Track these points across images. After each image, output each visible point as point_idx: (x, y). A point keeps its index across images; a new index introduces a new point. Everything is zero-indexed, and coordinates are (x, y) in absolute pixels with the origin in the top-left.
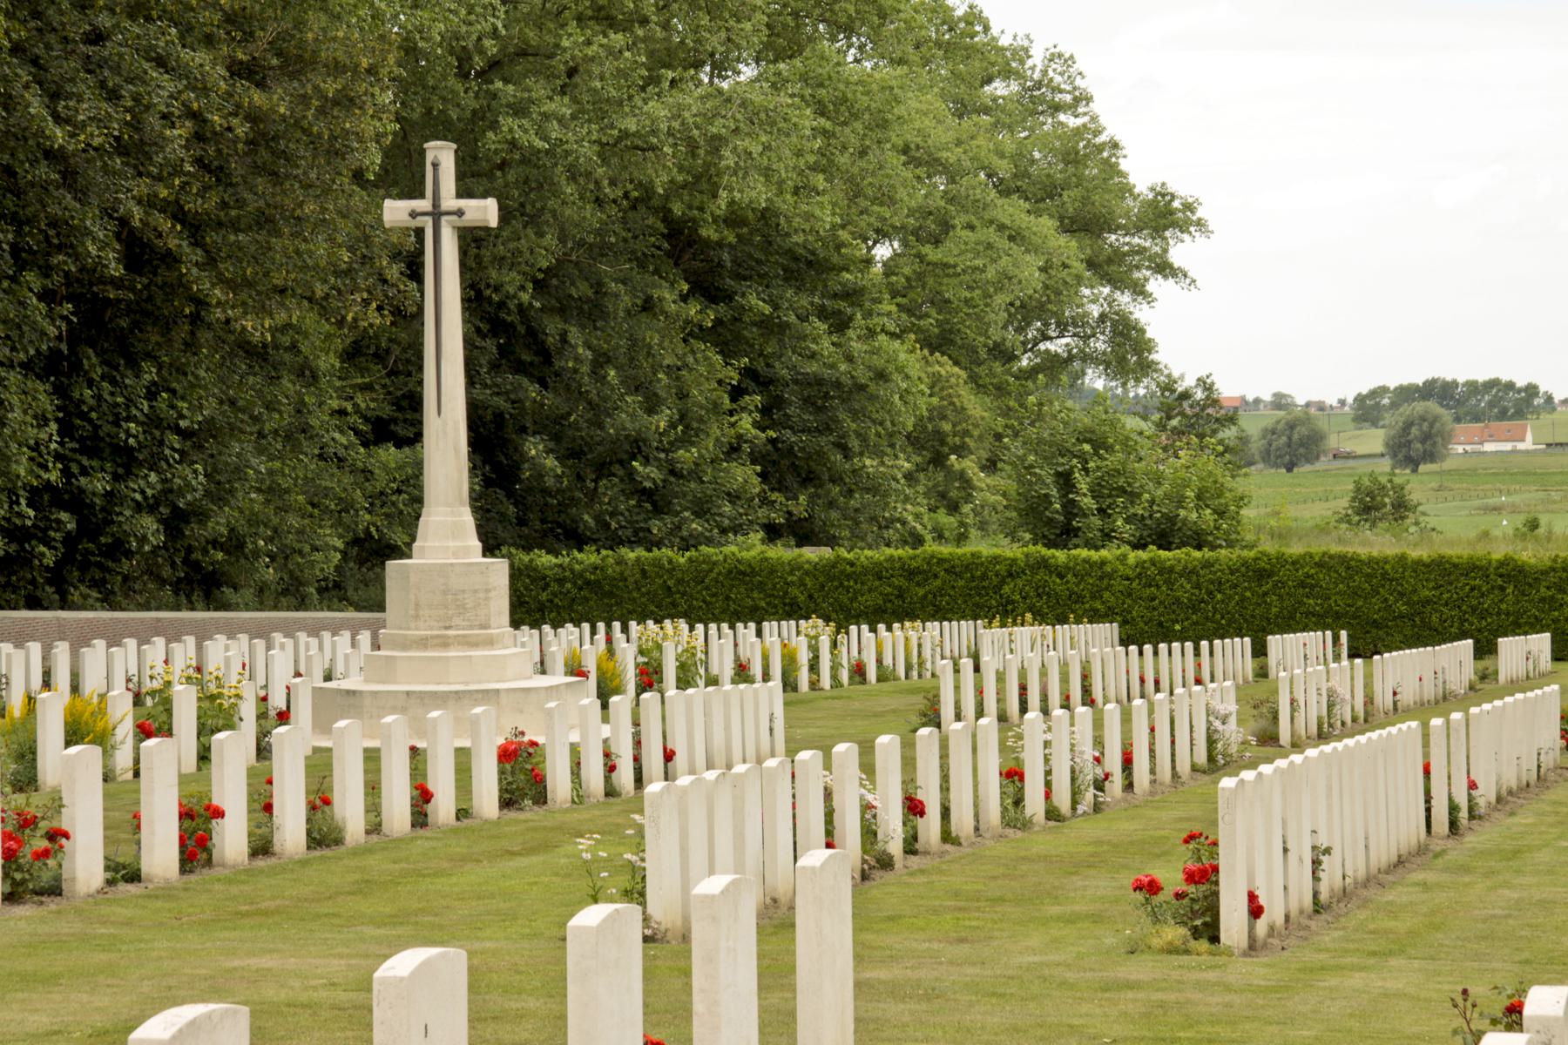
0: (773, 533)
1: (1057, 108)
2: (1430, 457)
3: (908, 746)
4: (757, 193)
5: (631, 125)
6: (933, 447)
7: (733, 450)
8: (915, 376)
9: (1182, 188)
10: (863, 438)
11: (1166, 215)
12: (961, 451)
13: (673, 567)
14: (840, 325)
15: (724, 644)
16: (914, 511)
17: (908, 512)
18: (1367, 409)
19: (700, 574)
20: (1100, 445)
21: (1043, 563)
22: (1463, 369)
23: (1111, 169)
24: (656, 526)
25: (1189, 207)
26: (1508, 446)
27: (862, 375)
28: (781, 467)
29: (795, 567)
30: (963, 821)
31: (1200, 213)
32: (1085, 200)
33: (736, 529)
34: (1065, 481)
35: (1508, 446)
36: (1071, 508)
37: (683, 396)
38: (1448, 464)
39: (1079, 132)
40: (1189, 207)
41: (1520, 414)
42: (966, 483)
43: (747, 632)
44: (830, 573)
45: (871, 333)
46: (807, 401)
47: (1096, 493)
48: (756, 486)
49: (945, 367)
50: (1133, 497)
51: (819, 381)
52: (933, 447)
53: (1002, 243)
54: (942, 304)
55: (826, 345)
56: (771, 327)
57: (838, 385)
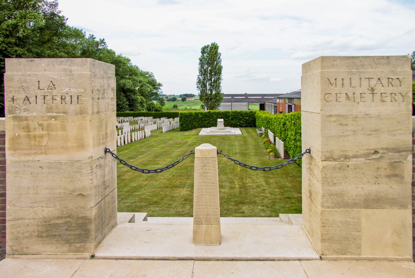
0: (129, 110)
1: (151, 77)
2: (185, 101)
3: (134, 125)
4: (128, 87)
5: (119, 82)
6: (141, 103)
7: (126, 105)
8: (139, 98)
9: (161, 83)
10: (136, 103)
11: (160, 85)
12: (144, 103)
13: (122, 113)
14: (134, 95)
15: (126, 119)
16: (140, 108)
17: (139, 108)
18: (181, 96)
19: (124, 113)
20: (152, 104)
21: (148, 113)
22: (188, 93)
23: (155, 81)
24: (121, 110)
25: (161, 84)
26: (191, 99)
27: (136, 99)
28: (130, 106)
29: (131, 113)
30: (137, 129)
31: (162, 85)
32: (154, 84)
33: (127, 110)
34: (150, 107)
35: (191, 99)
36: (150, 109)
37: (123, 101)
38: (186, 101)
39: (153, 79)
40: (161, 84)
41: (193, 97)
42: (144, 106)
43: (127, 118)
44: (133, 113)
45: (137, 96)
46: (132, 101)
47: (152, 107)
48: (128, 107)
49: (142, 97)
50: (154, 108)
51: (133, 99)
52: (141, 103)
53: (147, 87)
54: (142, 92)
55: (133, 96)
56: (129, 95)
57: (134, 99)
